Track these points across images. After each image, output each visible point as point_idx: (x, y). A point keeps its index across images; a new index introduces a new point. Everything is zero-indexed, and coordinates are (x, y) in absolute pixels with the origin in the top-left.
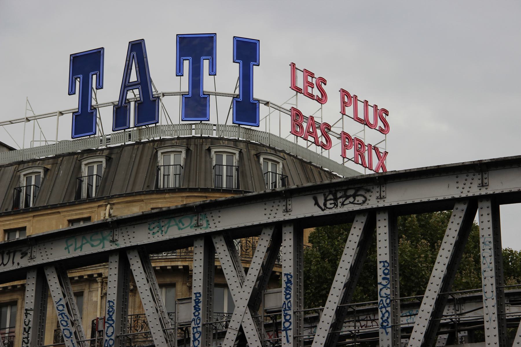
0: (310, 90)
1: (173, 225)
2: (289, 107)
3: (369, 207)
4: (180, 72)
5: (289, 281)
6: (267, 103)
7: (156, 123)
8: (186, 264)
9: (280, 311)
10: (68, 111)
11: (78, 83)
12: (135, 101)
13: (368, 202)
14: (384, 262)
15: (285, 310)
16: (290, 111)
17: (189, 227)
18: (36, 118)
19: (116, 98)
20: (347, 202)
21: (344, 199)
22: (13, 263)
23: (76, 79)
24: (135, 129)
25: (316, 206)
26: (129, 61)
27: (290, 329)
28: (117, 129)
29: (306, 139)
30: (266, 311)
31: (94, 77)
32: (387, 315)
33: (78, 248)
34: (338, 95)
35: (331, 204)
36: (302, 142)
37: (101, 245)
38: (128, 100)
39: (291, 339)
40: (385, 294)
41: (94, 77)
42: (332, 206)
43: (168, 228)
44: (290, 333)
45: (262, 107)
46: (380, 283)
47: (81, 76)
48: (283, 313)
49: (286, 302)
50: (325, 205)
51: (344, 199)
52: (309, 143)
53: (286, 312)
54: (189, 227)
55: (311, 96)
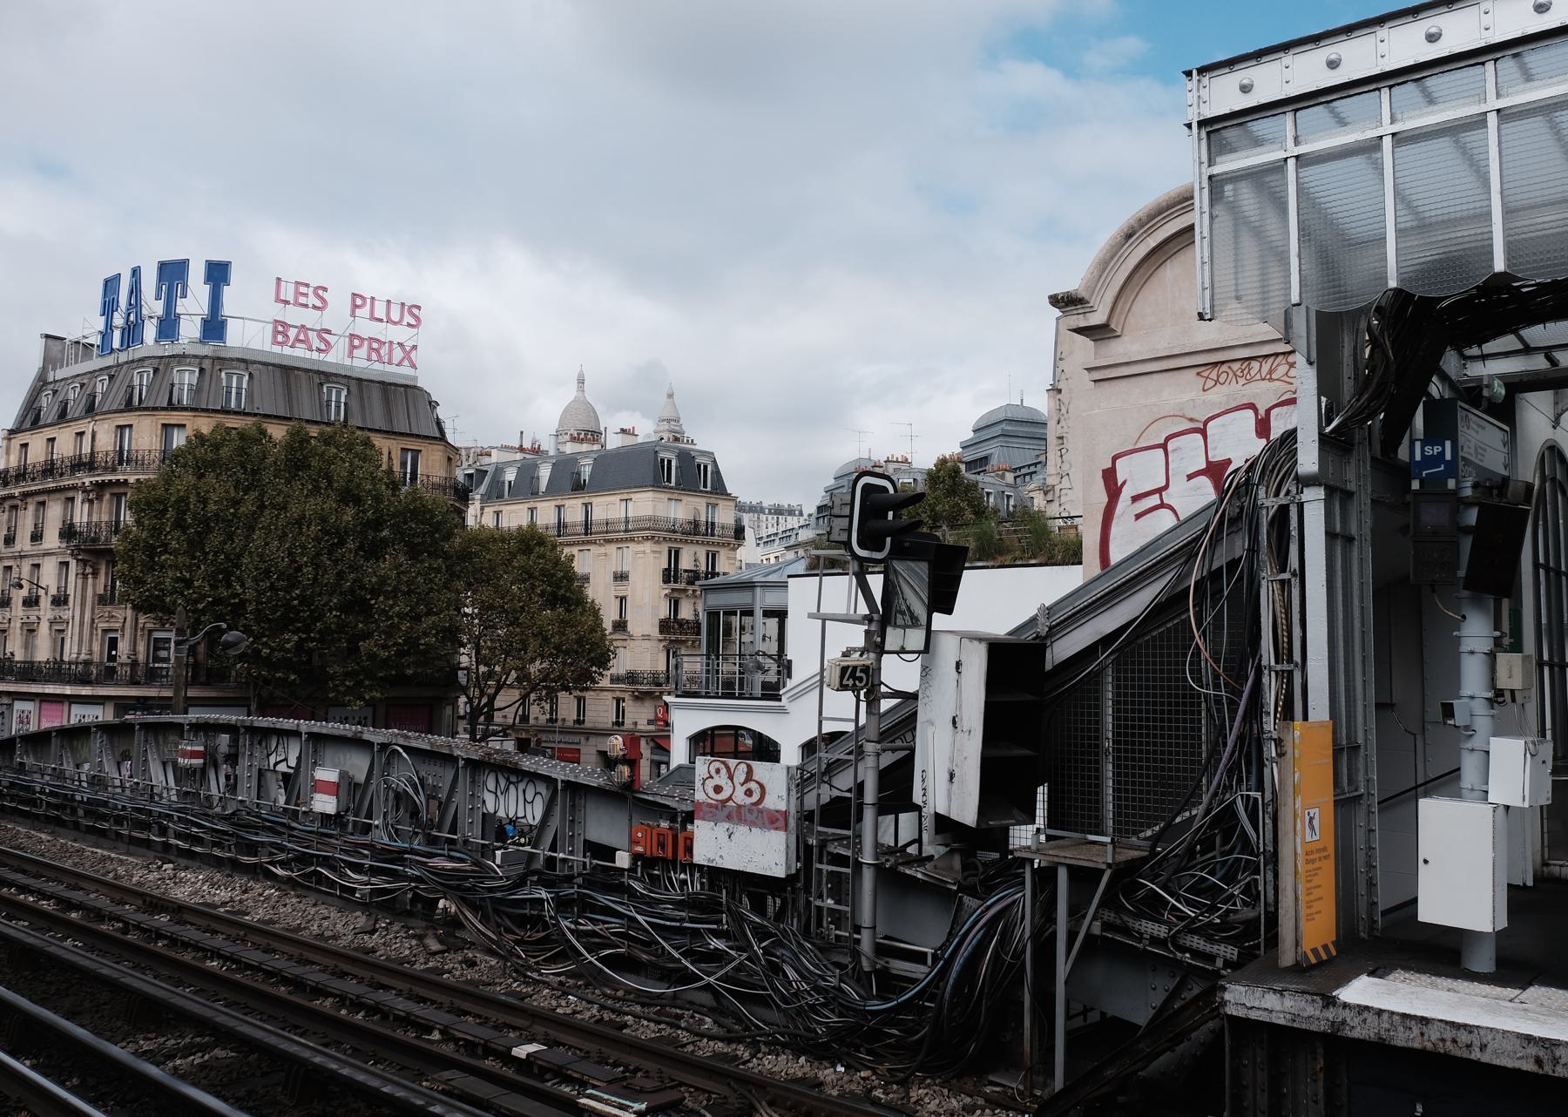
8: (125, 477)
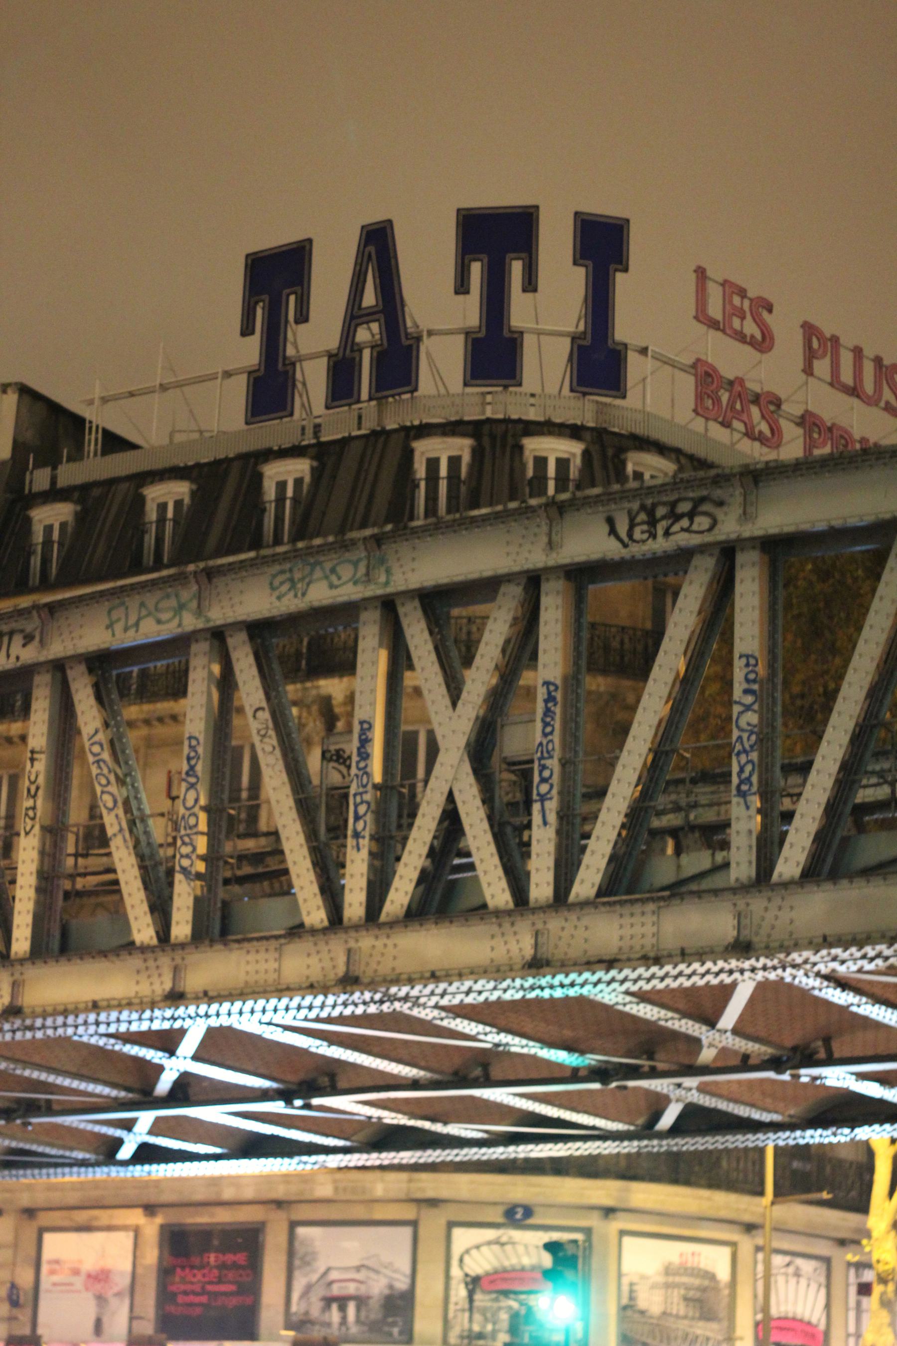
0: (736, 323)
1: (319, 580)
2: (687, 360)
3: (722, 538)
4: (462, 285)
5: (550, 698)
6: (644, 351)
7: (412, 392)
9: (531, 761)
10: (238, 372)
11: (259, 312)
12: (372, 347)
13: (718, 526)
14: (747, 657)
15: (542, 758)
16: (694, 366)
17: (351, 584)
18: (179, 385)
19: (333, 342)
20: (676, 528)
21: (670, 522)
22: (8, 656)
23: (257, 303)
24: (373, 403)
25: (612, 538)
26: (361, 265)
27: (551, 799)
28: (336, 403)
29: (726, 424)
30: (505, 760)
31: (292, 298)
32: (749, 768)
33: (132, 626)
34: (799, 337)
35: (643, 532)
36: (717, 432)
37: (176, 622)
38: (358, 344)
39: (552, 818)
40: (749, 724)
41: (292, 298)
42: (645, 536)
43: (308, 584)
44: (552, 806)
45: (632, 358)
46: (739, 703)
47: (266, 297)
48: (536, 765)
49: (545, 742)
50: (630, 535)
51: (670, 522)
52: (735, 434)
53: (543, 762)
54: (351, 584)
55: (741, 337)
